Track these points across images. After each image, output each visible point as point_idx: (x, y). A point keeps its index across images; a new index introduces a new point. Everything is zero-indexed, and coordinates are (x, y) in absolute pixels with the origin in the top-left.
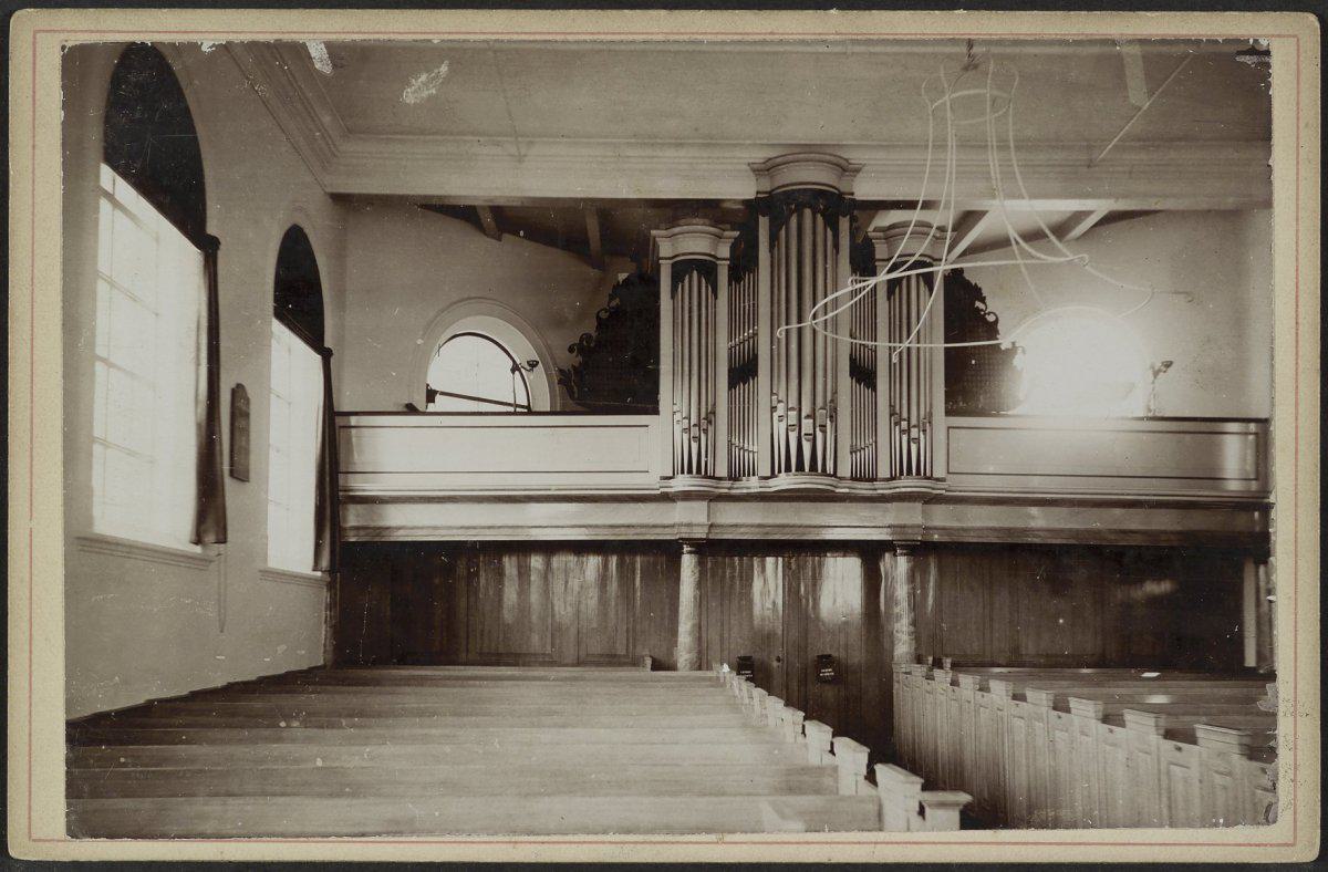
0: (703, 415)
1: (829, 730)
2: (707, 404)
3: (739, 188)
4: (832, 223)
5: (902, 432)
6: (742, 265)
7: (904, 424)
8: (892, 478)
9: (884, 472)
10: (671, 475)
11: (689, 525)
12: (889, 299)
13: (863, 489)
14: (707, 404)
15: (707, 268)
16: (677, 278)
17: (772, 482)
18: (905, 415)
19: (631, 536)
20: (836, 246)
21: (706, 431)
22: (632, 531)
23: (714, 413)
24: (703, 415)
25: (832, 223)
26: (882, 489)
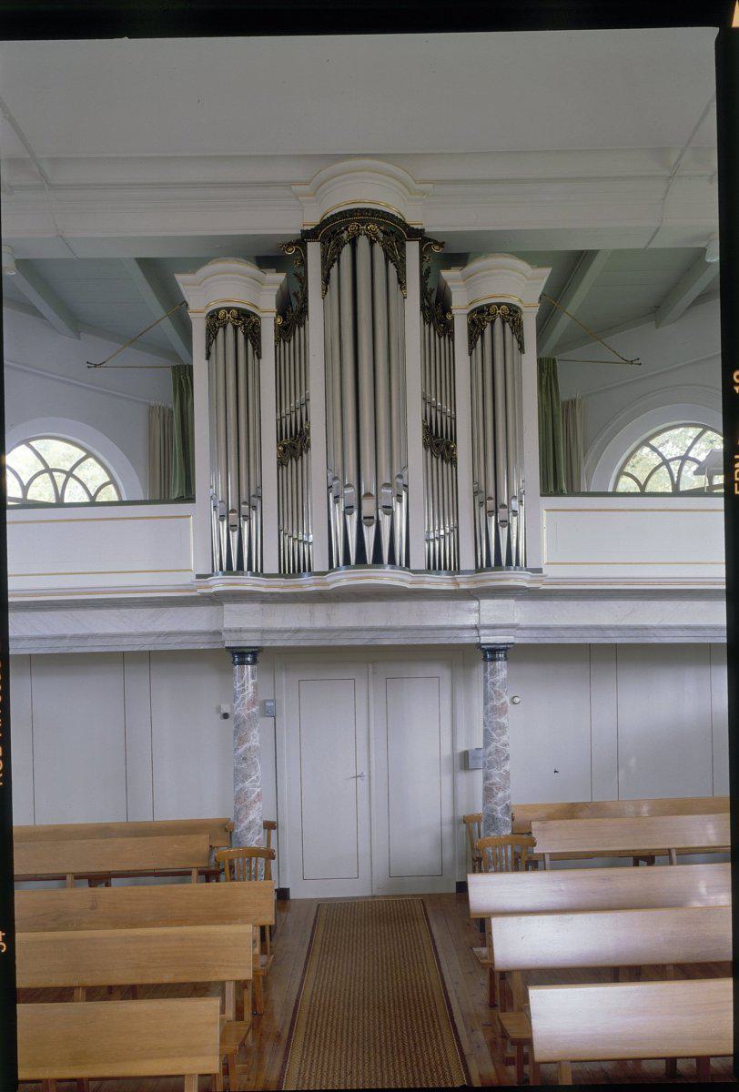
0: (244, 497)
1: (23, 447)
2: (300, 334)
3: (288, 221)
4: (395, 258)
5: (488, 513)
6: (292, 314)
7: (491, 504)
8: (479, 570)
9: (467, 562)
10: (211, 573)
11: (263, 631)
12: (470, 354)
13: (441, 582)
14: (300, 334)
15: (247, 322)
16: (211, 333)
17: (331, 578)
18: (491, 492)
19: (172, 645)
20: (402, 282)
21: (248, 518)
22: (549, 634)
23: (260, 498)
24: (244, 497)
25: (395, 258)
26: (464, 583)
